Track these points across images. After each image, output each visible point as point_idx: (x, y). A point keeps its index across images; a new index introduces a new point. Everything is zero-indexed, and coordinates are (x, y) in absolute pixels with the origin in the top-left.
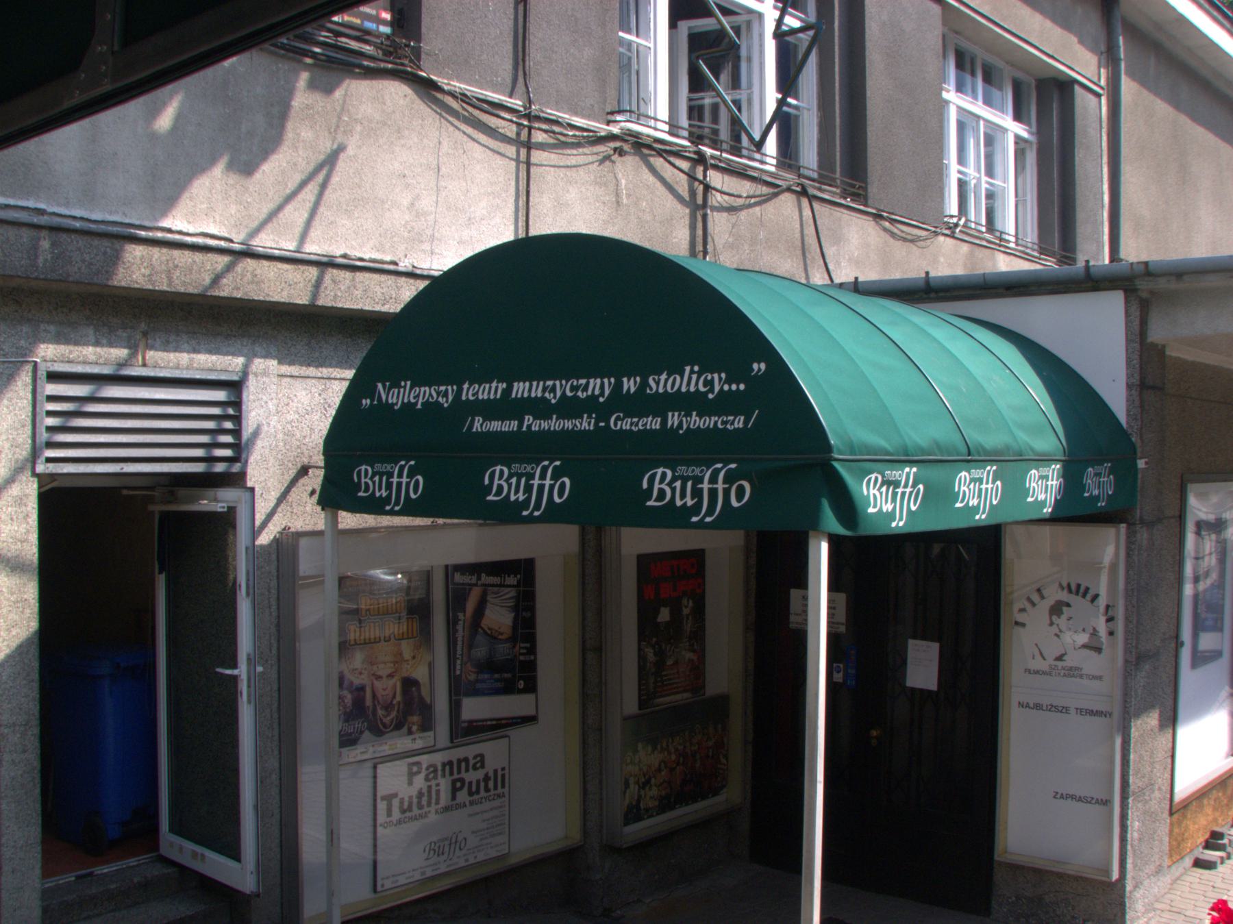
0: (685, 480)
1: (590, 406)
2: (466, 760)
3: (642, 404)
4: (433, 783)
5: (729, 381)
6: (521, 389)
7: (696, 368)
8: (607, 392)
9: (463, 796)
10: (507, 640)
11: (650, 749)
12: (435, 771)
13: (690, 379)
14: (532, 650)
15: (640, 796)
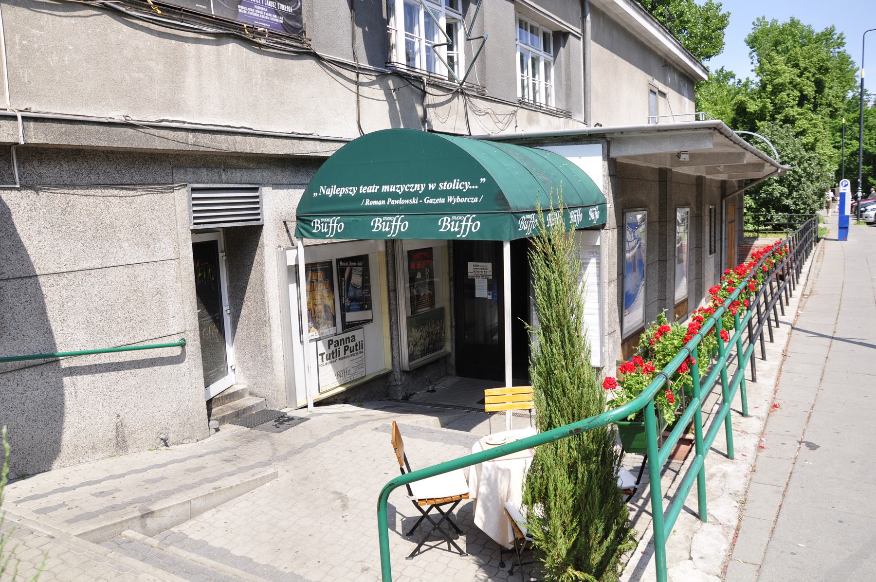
0: (456, 221)
1: (416, 194)
2: (349, 338)
3: (437, 194)
4: (337, 348)
5: (471, 185)
6: (385, 188)
7: (458, 180)
8: (422, 189)
9: (348, 352)
10: (360, 289)
11: (416, 331)
12: (338, 343)
13: (456, 184)
14: (369, 292)
15: (414, 350)
